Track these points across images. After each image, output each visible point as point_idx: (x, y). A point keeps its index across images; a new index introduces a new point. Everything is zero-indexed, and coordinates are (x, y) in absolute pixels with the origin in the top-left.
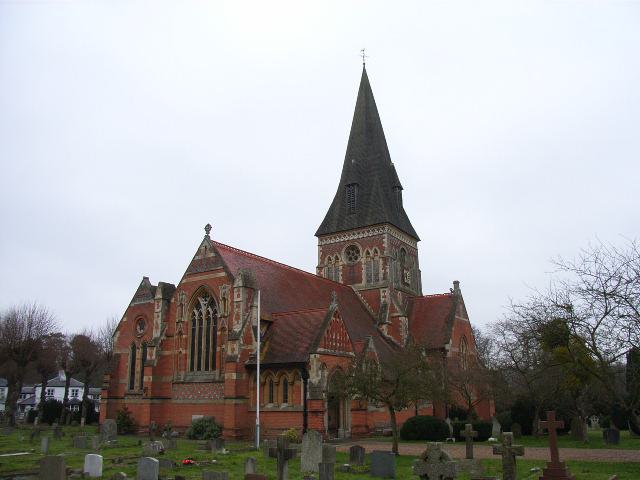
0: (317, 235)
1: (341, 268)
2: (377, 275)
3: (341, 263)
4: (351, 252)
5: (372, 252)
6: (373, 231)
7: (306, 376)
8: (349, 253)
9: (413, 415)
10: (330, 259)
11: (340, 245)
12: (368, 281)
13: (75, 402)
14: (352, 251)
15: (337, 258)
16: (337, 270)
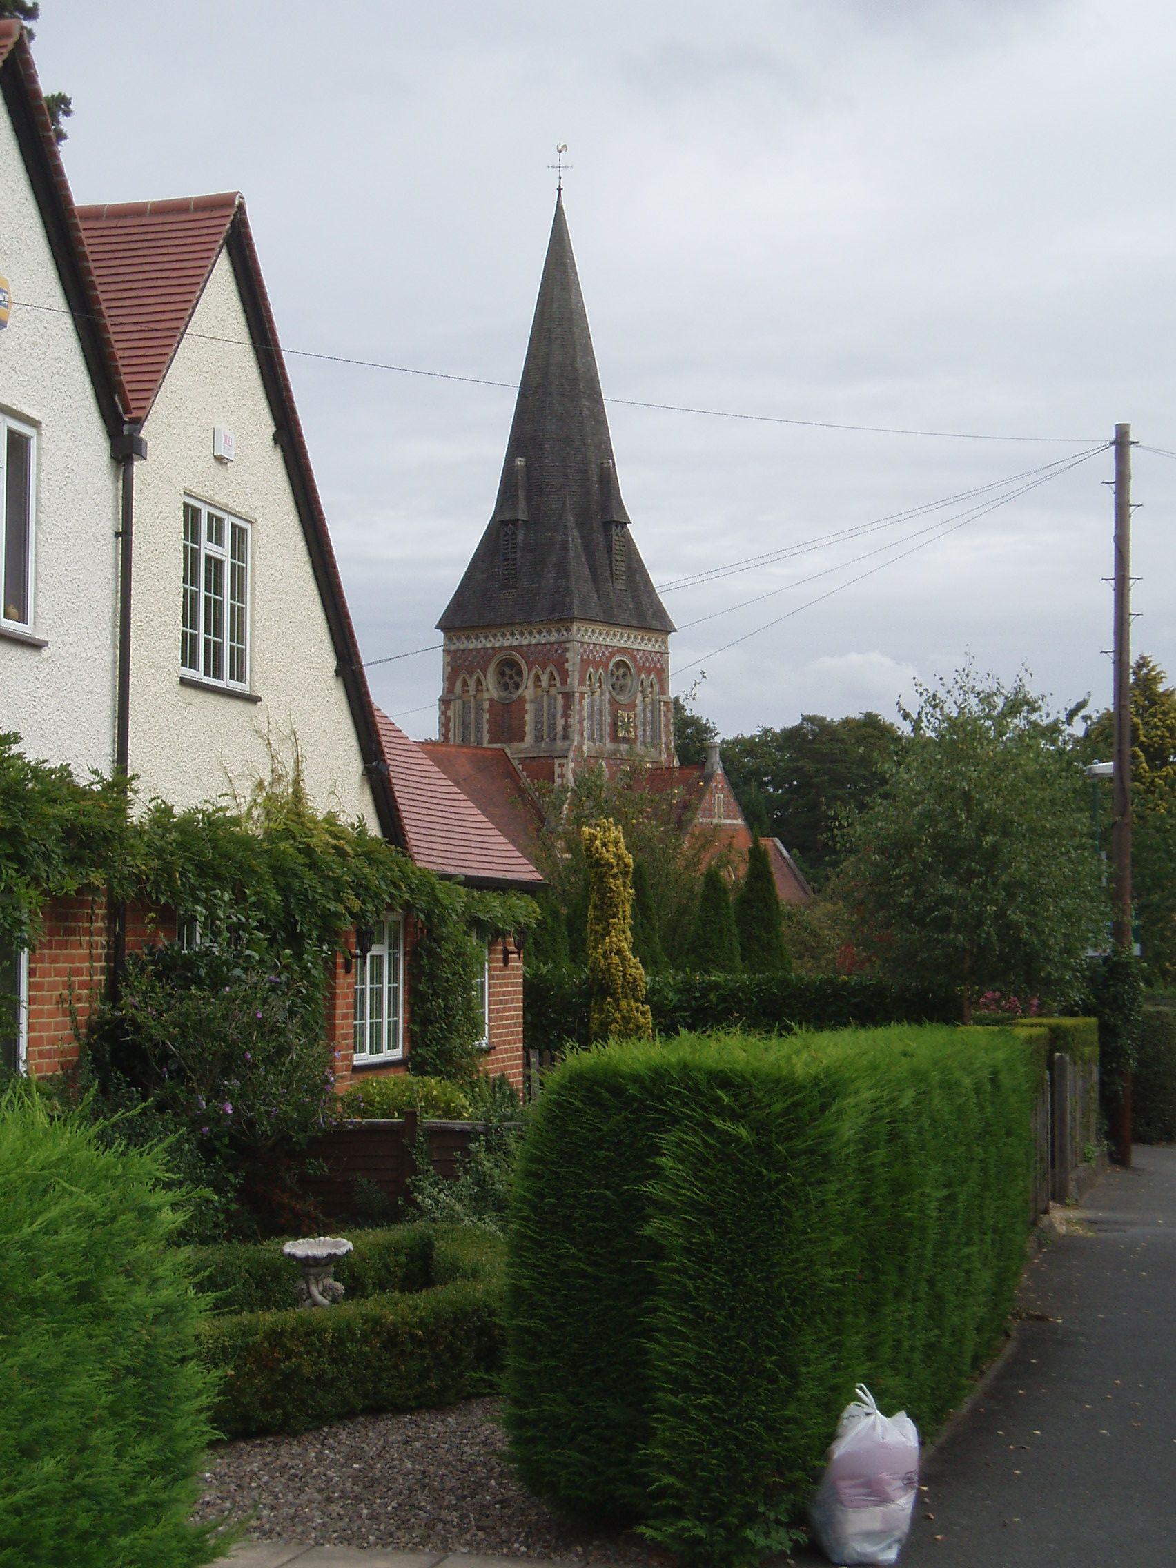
0: (441, 626)
1: (486, 705)
2: (552, 726)
3: (486, 695)
4: (508, 672)
5: (545, 679)
6: (549, 632)
7: (243, 968)
8: (503, 674)
9: (1132, 439)
10: (465, 683)
11: (488, 655)
12: (538, 739)
13: (524, 999)
14: (509, 671)
15: (479, 683)
16: (479, 709)
